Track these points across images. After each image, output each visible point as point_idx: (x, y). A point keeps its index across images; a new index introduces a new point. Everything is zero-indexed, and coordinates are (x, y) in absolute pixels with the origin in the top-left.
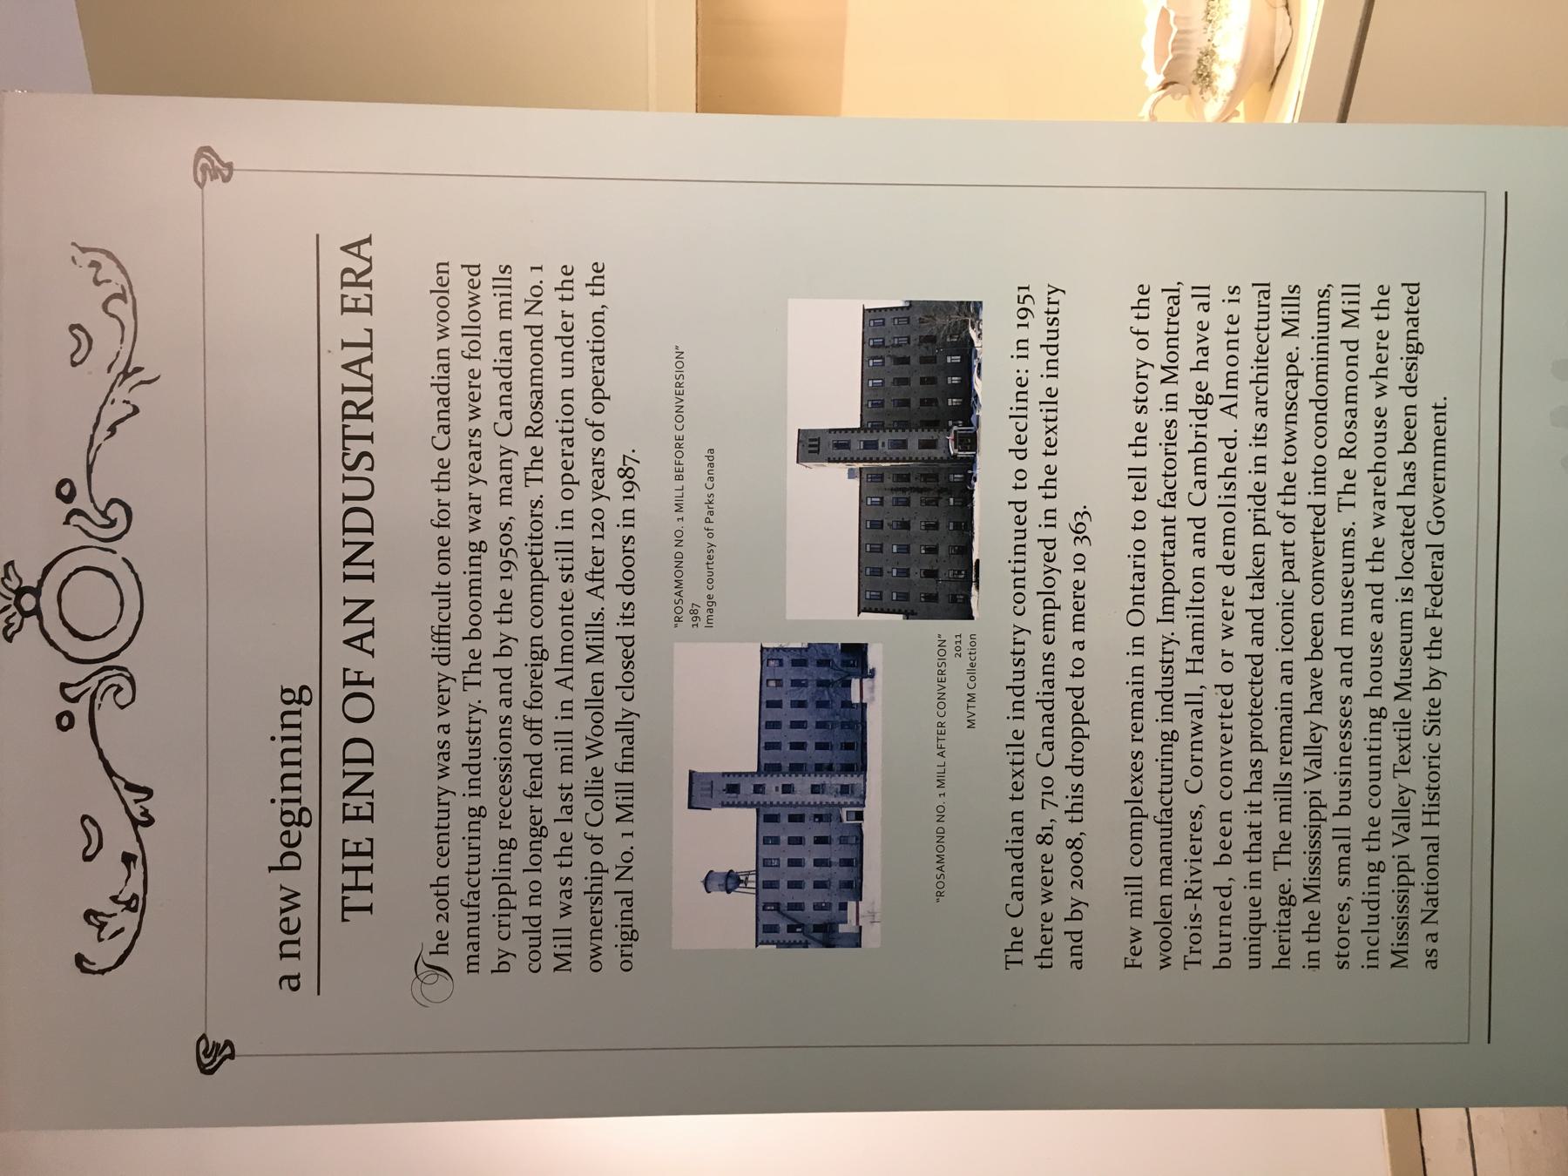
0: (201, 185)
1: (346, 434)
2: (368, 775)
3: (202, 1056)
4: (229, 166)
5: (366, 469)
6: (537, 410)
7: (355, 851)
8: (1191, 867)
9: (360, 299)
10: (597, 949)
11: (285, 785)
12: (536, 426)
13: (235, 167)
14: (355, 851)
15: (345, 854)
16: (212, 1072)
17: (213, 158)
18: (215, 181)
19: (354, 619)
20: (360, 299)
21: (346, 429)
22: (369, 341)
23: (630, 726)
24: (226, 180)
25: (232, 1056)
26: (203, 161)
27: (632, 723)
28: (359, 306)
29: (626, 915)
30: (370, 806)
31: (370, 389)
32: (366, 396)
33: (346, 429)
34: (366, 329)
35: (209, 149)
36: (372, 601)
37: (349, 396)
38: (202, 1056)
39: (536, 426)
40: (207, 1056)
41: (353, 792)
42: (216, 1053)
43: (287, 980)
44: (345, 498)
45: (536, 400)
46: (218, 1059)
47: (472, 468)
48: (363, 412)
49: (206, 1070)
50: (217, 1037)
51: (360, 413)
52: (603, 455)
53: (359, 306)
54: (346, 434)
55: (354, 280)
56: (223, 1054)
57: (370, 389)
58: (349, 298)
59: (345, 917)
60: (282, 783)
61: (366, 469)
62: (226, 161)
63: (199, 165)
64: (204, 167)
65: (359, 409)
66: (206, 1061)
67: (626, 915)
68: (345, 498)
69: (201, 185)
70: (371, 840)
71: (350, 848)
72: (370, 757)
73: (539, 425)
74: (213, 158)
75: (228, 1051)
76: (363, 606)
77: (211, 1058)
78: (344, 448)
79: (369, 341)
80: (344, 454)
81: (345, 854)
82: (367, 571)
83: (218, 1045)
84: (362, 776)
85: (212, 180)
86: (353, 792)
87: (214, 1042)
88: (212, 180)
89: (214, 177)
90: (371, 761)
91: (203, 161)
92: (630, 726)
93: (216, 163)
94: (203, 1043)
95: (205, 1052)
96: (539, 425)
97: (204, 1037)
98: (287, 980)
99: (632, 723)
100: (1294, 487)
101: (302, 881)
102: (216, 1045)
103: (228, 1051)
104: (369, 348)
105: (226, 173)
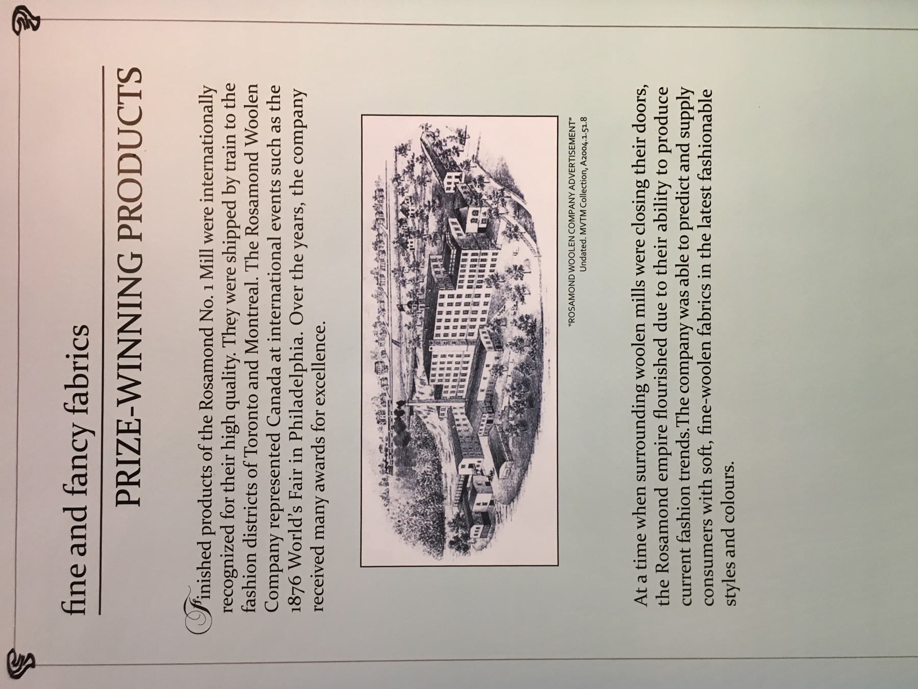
0: (18, 33)
1: (121, 92)
2: (137, 317)
3: (11, 666)
4: (38, 19)
5: (136, 82)
6: (254, 215)
7: (127, 429)
8: (704, 503)
9: (131, 423)
10: (321, 475)
11: (75, 464)
12: (253, 227)
13: (41, 18)
14: (127, 429)
15: (119, 431)
16: (18, 677)
17: (26, 14)
18: (27, 30)
19: (127, 293)
20: (131, 423)
21: (120, 88)
22: (138, 429)
23: (210, 99)
24: (35, 28)
25: (33, 665)
26: (19, 15)
27: (211, 97)
28: (130, 429)
29: (275, 400)
30: (138, 442)
31: (138, 462)
32: (135, 468)
33: (120, 88)
34: (135, 439)
35: (24, 8)
36: (140, 383)
37: (122, 467)
38: (11, 666)
39: (253, 227)
40: (15, 665)
41: (125, 330)
42: (21, 663)
43: (77, 548)
44: (120, 147)
45: (253, 208)
46: (23, 667)
47: (296, 236)
48: (132, 480)
49: (14, 676)
50: (22, 651)
51: (132, 215)
52: (302, 213)
53: (130, 429)
54: (121, 92)
55: (128, 215)
56: (27, 664)
57: (138, 462)
58: (123, 422)
59: (121, 101)
60: (73, 464)
61: (136, 82)
62: (35, 15)
63: (17, 19)
64: (20, 19)
65: (129, 477)
66: (14, 669)
67: (275, 400)
68: (120, 147)
69: (18, 33)
70: (139, 420)
71: (123, 426)
72: (139, 169)
73: (256, 226)
74: (26, 14)
75: (30, 662)
76: (132, 283)
77: (18, 667)
78: (119, 103)
79: (138, 429)
80: (119, 108)
81: (119, 431)
82: (136, 362)
83: (23, 657)
84: (133, 317)
85: (25, 29)
86: (125, 330)
87: (20, 655)
88: (25, 29)
89: (26, 27)
90: (140, 171)
91: (19, 15)
92: (210, 99)
93: (29, 17)
94: (12, 655)
95: (13, 662)
96: (256, 226)
97: (13, 651)
98: (77, 548)
99: (211, 97)
100: (644, 508)
101: (90, 501)
102: (21, 657)
103: (30, 662)
104: (138, 465)
105: (35, 23)
